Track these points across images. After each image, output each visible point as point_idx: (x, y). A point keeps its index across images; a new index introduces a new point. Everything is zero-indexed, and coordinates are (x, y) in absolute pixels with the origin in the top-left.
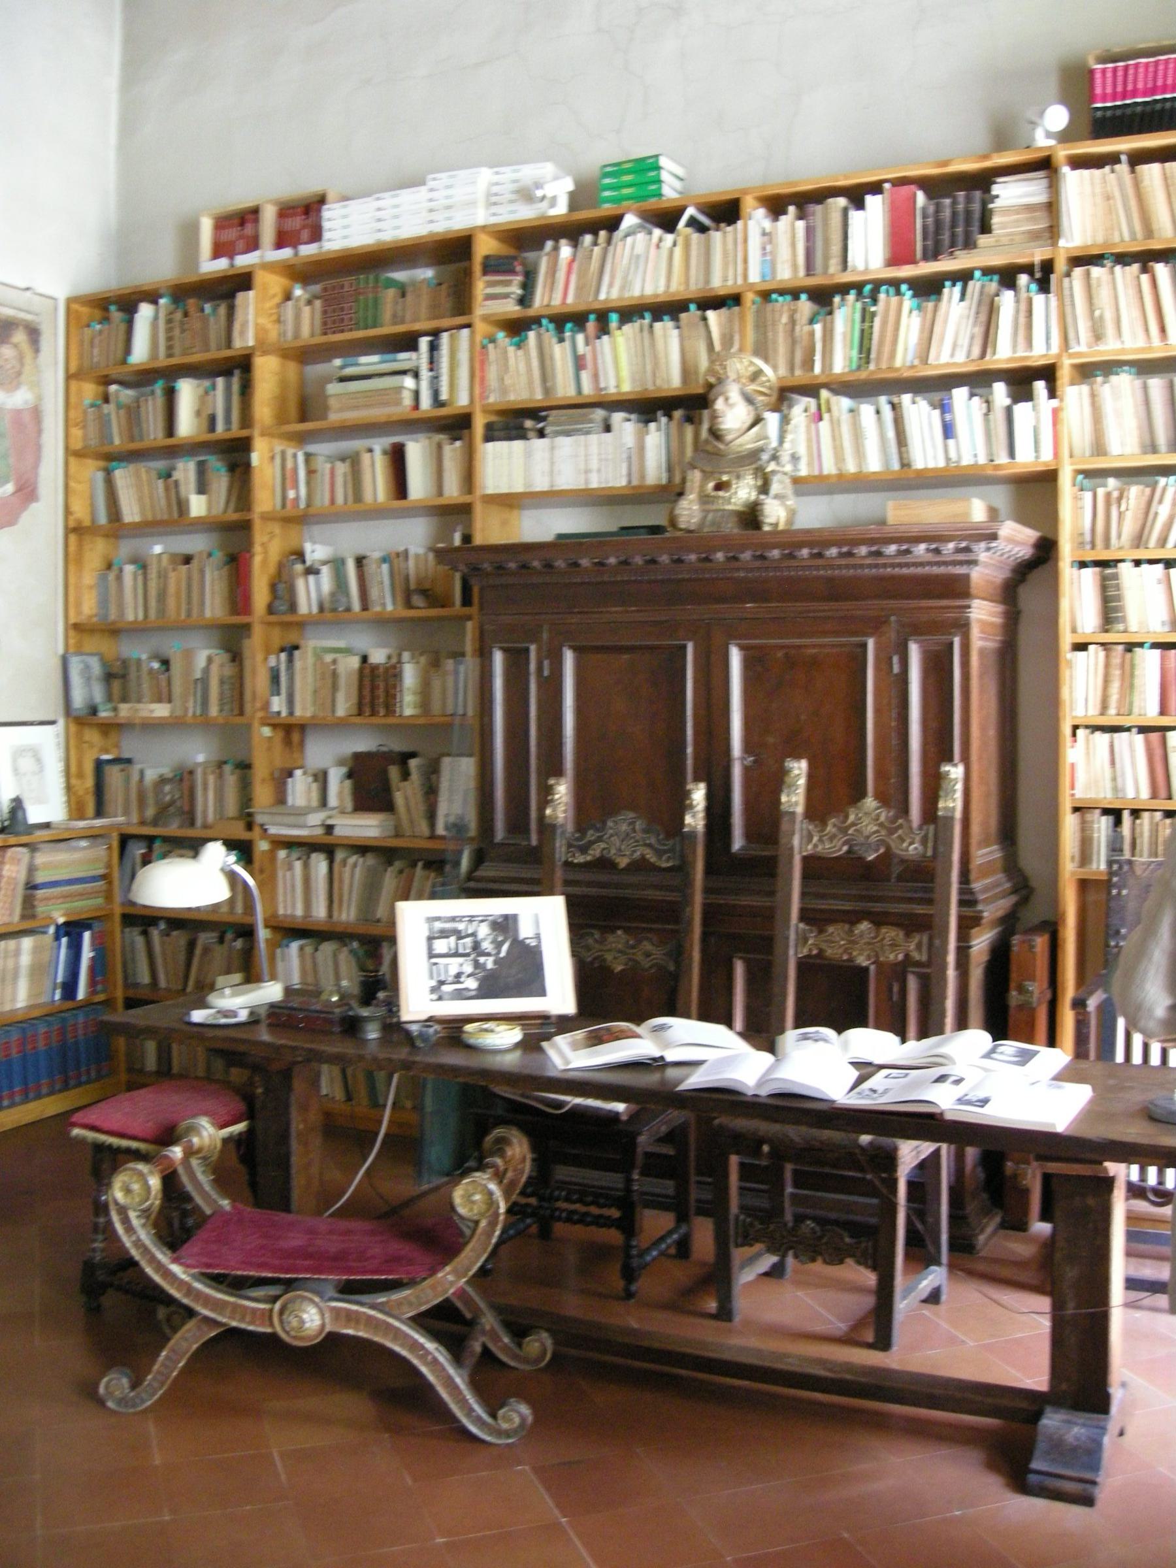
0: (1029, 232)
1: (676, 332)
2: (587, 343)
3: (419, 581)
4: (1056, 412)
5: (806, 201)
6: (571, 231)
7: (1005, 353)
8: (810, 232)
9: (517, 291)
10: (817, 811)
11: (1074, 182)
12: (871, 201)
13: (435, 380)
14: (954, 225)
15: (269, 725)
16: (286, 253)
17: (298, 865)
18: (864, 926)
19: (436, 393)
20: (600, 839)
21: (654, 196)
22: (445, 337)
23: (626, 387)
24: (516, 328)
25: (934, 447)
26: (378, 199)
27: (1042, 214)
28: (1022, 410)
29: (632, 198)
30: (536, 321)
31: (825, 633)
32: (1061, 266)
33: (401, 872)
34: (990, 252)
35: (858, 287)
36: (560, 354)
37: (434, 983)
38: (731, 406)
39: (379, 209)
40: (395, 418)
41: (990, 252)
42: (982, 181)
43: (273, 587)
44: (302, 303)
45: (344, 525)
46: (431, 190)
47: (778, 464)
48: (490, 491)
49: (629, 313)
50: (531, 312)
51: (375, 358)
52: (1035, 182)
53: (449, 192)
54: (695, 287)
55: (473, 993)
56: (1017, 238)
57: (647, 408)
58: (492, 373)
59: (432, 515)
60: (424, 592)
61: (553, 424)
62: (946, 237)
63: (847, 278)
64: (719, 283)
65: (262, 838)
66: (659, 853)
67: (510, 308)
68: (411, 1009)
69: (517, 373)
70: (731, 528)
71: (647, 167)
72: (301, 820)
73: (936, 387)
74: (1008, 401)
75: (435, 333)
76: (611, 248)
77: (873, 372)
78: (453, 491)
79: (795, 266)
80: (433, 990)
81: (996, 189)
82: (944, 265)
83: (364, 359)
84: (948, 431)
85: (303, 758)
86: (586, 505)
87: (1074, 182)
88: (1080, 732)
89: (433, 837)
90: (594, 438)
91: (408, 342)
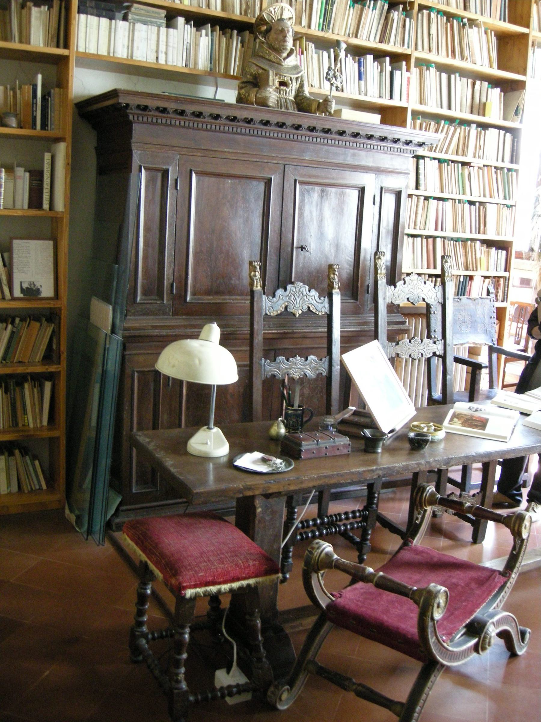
4: (409, 78)
48: (81, 49)
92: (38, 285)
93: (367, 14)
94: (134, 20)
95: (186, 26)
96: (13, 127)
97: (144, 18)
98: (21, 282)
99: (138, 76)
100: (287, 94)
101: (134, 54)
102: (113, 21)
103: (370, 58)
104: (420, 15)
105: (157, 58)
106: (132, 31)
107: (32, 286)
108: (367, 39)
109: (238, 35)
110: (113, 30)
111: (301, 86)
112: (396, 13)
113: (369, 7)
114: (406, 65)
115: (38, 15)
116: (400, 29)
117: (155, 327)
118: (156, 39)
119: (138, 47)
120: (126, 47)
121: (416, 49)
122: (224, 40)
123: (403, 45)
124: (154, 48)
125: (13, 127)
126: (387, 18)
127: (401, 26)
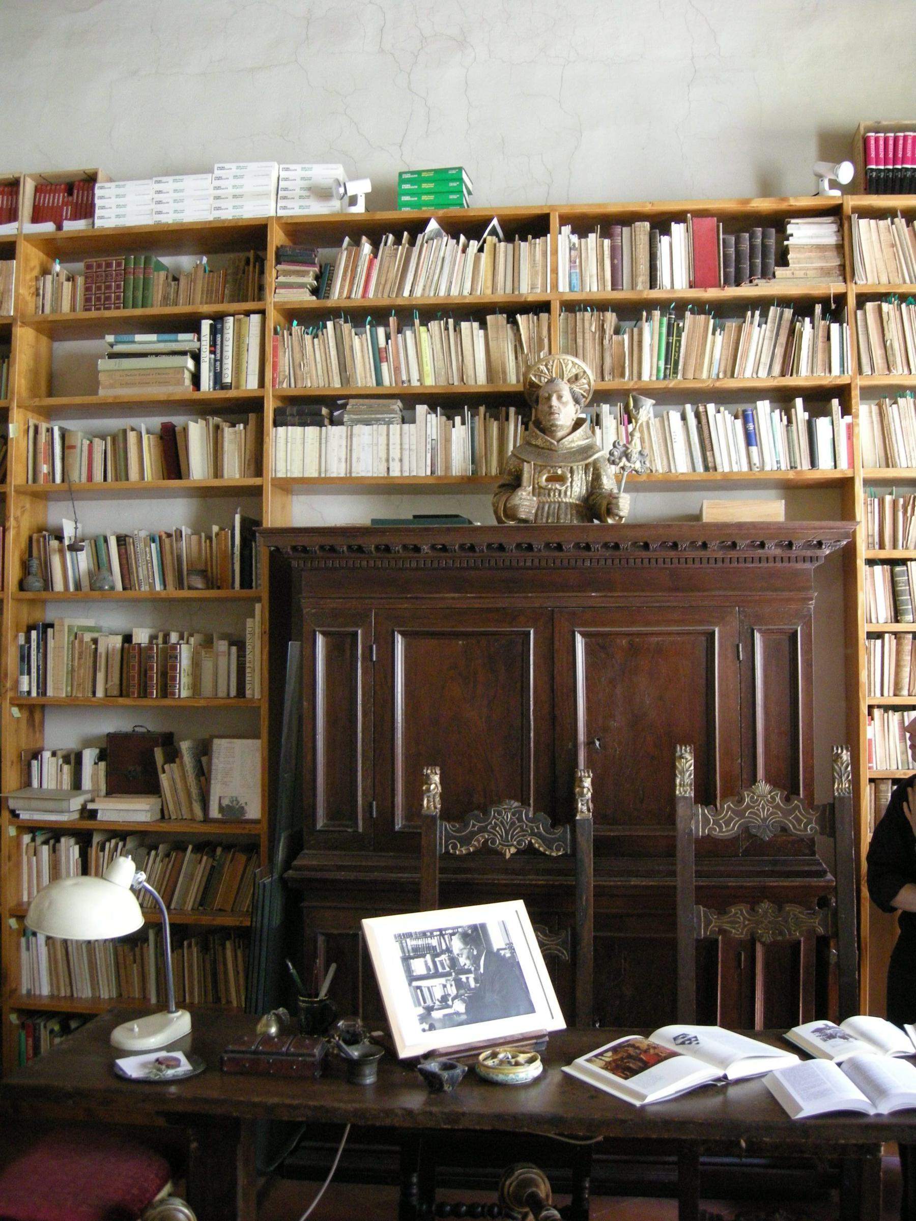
0: (822, 268)
1: (482, 332)
2: (388, 337)
3: (191, 563)
4: (850, 428)
6: (374, 231)
7: (806, 375)
8: (615, 252)
9: (310, 280)
10: (705, 793)
11: (865, 229)
12: (677, 229)
13: (217, 364)
14: (752, 256)
15: (18, 705)
16: (48, 227)
17: (45, 849)
18: (765, 906)
19: (218, 377)
20: (482, 830)
21: (456, 205)
23: (429, 381)
24: (312, 319)
25: (737, 451)
26: (159, 182)
27: (833, 254)
28: (822, 424)
29: (432, 205)
30: (334, 313)
31: (669, 622)
32: (851, 301)
33: (168, 855)
34: (786, 282)
35: (663, 305)
36: (360, 344)
37: (421, 1011)
38: (565, 404)
39: (159, 192)
40: (177, 398)
42: (778, 222)
43: (25, 567)
44: (63, 278)
45: (94, 503)
46: (219, 178)
47: (629, 460)
48: (281, 474)
49: (430, 313)
51: (153, 337)
52: (826, 226)
53: (238, 182)
54: (502, 294)
55: (464, 1017)
56: (810, 273)
57: (449, 403)
58: (285, 361)
59: (191, 496)
60: (203, 573)
61: (349, 413)
62: (746, 266)
63: (655, 294)
64: (528, 290)
65: (11, 823)
66: (549, 843)
67: (304, 298)
68: (408, 1043)
69: (313, 361)
70: (568, 519)
71: (448, 178)
72: (64, 805)
73: (739, 399)
74: (806, 415)
75: (218, 319)
77: (680, 382)
78: (234, 471)
79: (601, 278)
80: (423, 1018)
81: (790, 229)
83: (139, 338)
84: (750, 439)
85: (43, 738)
86: (378, 494)
87: (865, 229)
88: (877, 713)
89: (207, 820)
91: (191, 324)
92: (242, 802)
93: (750, 334)
94: (352, 422)
96: (197, 589)
98: (220, 798)
99: (402, 494)
102: (324, 428)
103: (763, 406)
105: (388, 469)
106: (350, 437)
107: (235, 803)
108: (755, 376)
109: (517, 414)
110: (323, 441)
111: (597, 477)
112: (807, 320)
113: (752, 323)
115: (233, 437)
116: (820, 345)
117: (339, 868)
118: (385, 442)
119: (358, 459)
120: (343, 460)
121: (860, 371)
122: (495, 426)
124: (383, 455)
125: (197, 589)
126: (792, 331)
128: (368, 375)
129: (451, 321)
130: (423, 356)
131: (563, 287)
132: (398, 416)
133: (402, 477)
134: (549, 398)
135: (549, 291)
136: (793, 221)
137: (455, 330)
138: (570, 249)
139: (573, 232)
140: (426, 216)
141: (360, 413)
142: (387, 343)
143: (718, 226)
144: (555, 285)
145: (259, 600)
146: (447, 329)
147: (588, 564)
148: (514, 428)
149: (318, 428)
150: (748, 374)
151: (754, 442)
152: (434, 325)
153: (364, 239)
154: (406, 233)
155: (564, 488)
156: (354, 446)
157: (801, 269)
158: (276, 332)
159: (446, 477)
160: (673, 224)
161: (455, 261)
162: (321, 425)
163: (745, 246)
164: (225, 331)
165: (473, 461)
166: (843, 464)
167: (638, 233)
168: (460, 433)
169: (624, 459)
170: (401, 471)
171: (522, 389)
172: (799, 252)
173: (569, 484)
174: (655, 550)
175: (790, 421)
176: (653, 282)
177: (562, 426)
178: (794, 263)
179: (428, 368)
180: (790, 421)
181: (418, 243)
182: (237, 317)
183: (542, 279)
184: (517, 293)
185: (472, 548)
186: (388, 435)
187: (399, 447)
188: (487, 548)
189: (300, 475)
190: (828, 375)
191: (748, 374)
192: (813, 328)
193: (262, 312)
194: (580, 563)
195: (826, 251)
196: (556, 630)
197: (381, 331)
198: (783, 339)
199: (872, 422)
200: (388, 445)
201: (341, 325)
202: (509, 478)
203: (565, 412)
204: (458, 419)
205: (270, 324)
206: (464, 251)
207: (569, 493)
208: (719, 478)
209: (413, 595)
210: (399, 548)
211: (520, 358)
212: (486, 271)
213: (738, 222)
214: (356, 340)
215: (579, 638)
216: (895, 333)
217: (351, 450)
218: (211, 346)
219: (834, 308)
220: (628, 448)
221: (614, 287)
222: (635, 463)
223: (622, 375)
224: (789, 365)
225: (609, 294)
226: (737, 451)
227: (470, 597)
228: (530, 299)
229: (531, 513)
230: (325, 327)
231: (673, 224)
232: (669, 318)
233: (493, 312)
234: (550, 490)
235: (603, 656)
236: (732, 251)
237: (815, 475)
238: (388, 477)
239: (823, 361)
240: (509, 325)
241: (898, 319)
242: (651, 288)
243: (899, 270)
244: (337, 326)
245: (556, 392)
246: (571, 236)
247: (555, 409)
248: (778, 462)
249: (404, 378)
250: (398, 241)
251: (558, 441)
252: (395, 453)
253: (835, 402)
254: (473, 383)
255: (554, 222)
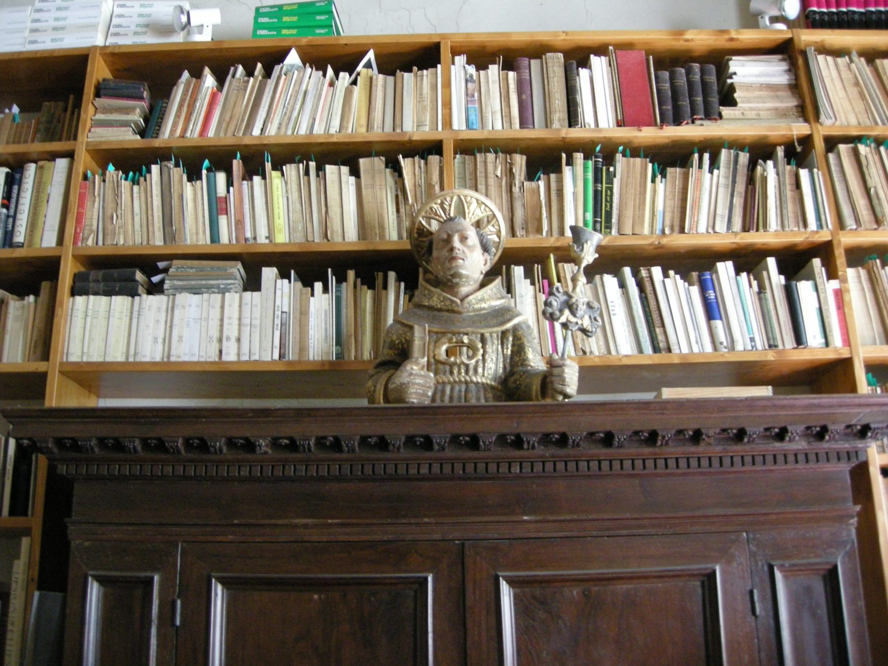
0: (776, 109)
1: (352, 179)
2: (230, 183)
4: (839, 295)
5: (510, 57)
7: (775, 232)
9: (137, 117)
22: (31, 169)
23: (282, 238)
24: (132, 163)
25: (697, 327)
28: (804, 288)
30: (161, 155)
32: (819, 145)
34: (731, 125)
35: (588, 149)
36: (192, 196)
41: (731, 125)
47: (573, 314)
50: (157, 143)
54: (381, 130)
56: (763, 114)
57: (308, 267)
58: (93, 213)
62: (685, 103)
63: (575, 133)
67: (127, 137)
69: (130, 216)
73: (695, 264)
76: (271, 83)
77: (615, 238)
79: (506, 116)
82: (688, 131)
84: (712, 310)
90: (232, 298)
93: (699, 181)
95: (279, 281)
97: (193, 283)
100: (471, 372)
101: (173, 352)
102: (137, 298)
104: (831, 156)
105: (221, 351)
108: (710, 230)
110: (135, 314)
111: (519, 350)
112: (770, 163)
113: (700, 166)
114: (823, 265)
118: (218, 316)
119: (180, 338)
120: (160, 340)
121: (841, 224)
123: (805, 225)
124: (215, 334)
126: (751, 180)
127: (788, 187)
128: (201, 231)
129: (312, 164)
130: (275, 208)
131: (459, 123)
132: (238, 283)
133: (239, 362)
134: (449, 240)
135: (440, 128)
136: (734, 58)
137: (318, 176)
138: (467, 81)
139: (469, 62)
140: (286, 44)
141: (187, 278)
142: (228, 191)
143: (648, 60)
144: (448, 122)
145: (27, 532)
146: (307, 173)
147: (516, 469)
148: (394, 298)
149: (130, 298)
150: (702, 229)
151: (717, 315)
152: (290, 170)
153: (207, 70)
154: (259, 65)
155: (473, 362)
156: (176, 321)
157: (751, 109)
158: (85, 178)
159: (299, 362)
160: (592, 56)
161: (320, 95)
162: (133, 294)
163: (682, 81)
164: (24, 180)
165: (339, 342)
166: (837, 339)
167: (550, 65)
168: (320, 302)
169: (567, 312)
170: (239, 355)
171: (407, 246)
172: (747, 90)
173: (480, 357)
174: (620, 446)
175: (761, 288)
176: (573, 118)
177: (467, 277)
178: (743, 102)
179: (280, 221)
180: (761, 288)
181: (275, 75)
182: (41, 163)
183: (431, 116)
184: (398, 131)
185: (337, 445)
186: (222, 307)
187: (236, 322)
188: (359, 444)
189: (101, 360)
190: (802, 230)
191: (702, 229)
192: (778, 174)
193: (70, 155)
194: (504, 468)
195: (778, 90)
196: (469, 576)
197: (221, 177)
198: (741, 187)
199: (863, 289)
200: (222, 320)
201: (169, 169)
202: (392, 352)
203: (473, 262)
204: (318, 286)
205: (80, 168)
206: (332, 84)
207: (480, 370)
208: (676, 361)
209: (243, 522)
210: (221, 443)
211: (402, 210)
212: (359, 107)
213: (669, 61)
214: (188, 187)
215: (505, 588)
216: (877, 179)
217: (171, 327)
218: (3, 198)
219: (799, 153)
220: (570, 297)
221: (523, 124)
222: (582, 318)
223: (539, 230)
224: (752, 217)
225: (516, 131)
226: (697, 327)
227: (331, 524)
228: (416, 137)
229: (425, 395)
230: (149, 171)
231: (592, 56)
232: (596, 161)
233: (368, 155)
234: (452, 365)
235: (541, 614)
236: (667, 86)
237: (802, 356)
238: (221, 362)
239: (795, 213)
240: (388, 170)
241: (879, 165)
242: (570, 126)
243: (868, 110)
244: (165, 170)
245: (458, 231)
246: (467, 66)
247: (458, 253)
248: (752, 340)
249: (249, 235)
250: (250, 73)
251: (462, 300)
252: (231, 331)
253: (817, 262)
254: (340, 240)
255: (445, 53)
